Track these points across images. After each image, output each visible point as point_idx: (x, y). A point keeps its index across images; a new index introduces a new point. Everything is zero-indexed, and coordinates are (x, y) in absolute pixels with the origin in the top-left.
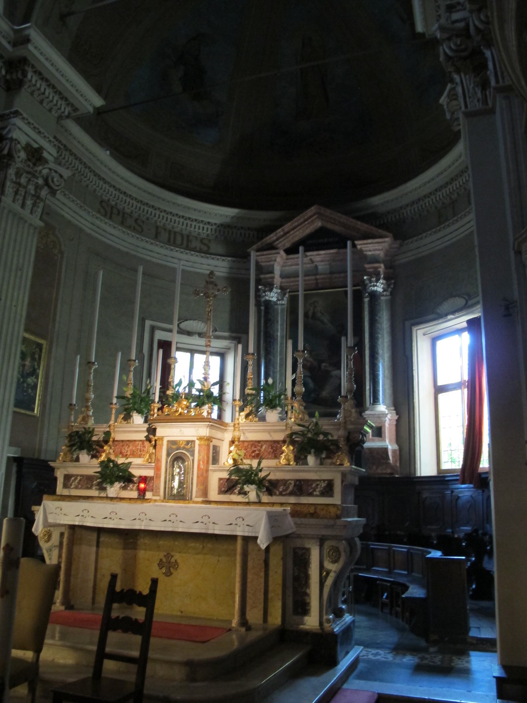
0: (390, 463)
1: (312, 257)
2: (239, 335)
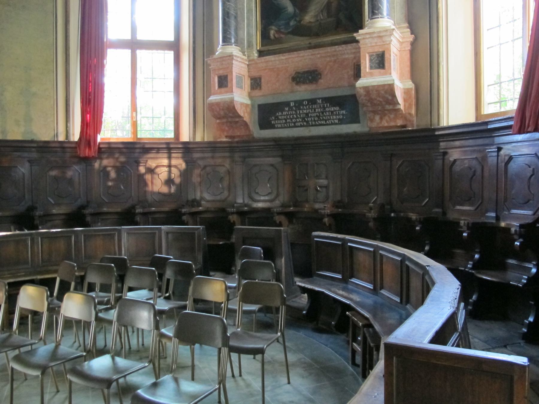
0: (399, 110)
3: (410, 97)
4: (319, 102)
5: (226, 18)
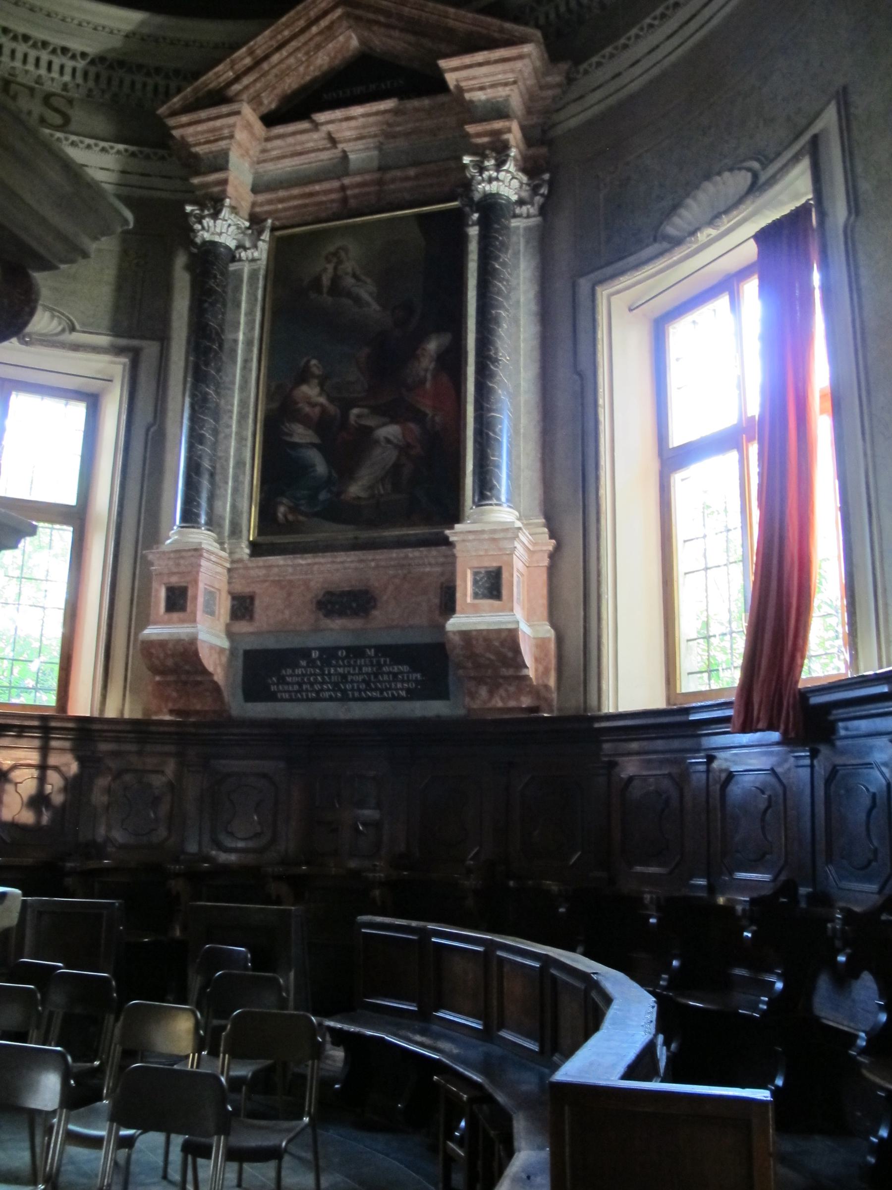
0: (526, 677)
1: (330, 127)
2: (135, 343)
3: (546, 655)
4: (369, 653)
5: (193, 474)
